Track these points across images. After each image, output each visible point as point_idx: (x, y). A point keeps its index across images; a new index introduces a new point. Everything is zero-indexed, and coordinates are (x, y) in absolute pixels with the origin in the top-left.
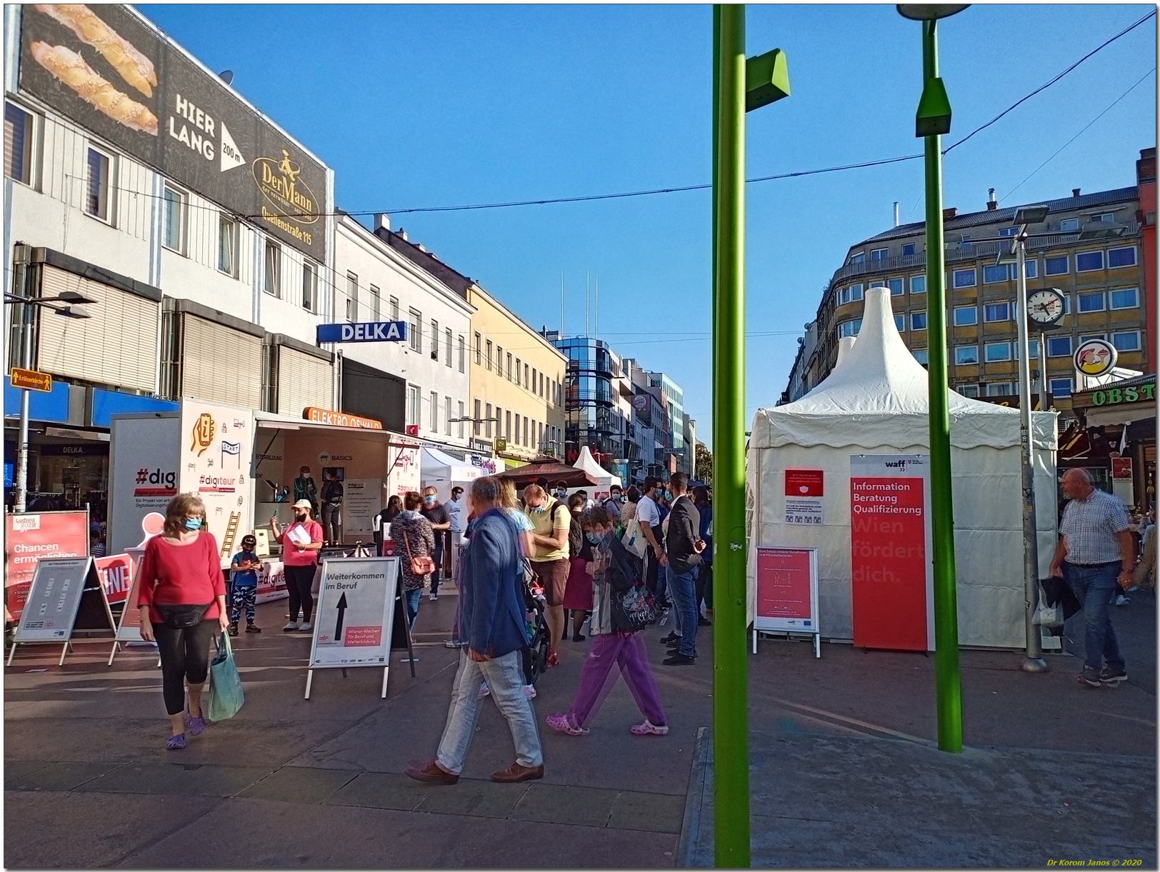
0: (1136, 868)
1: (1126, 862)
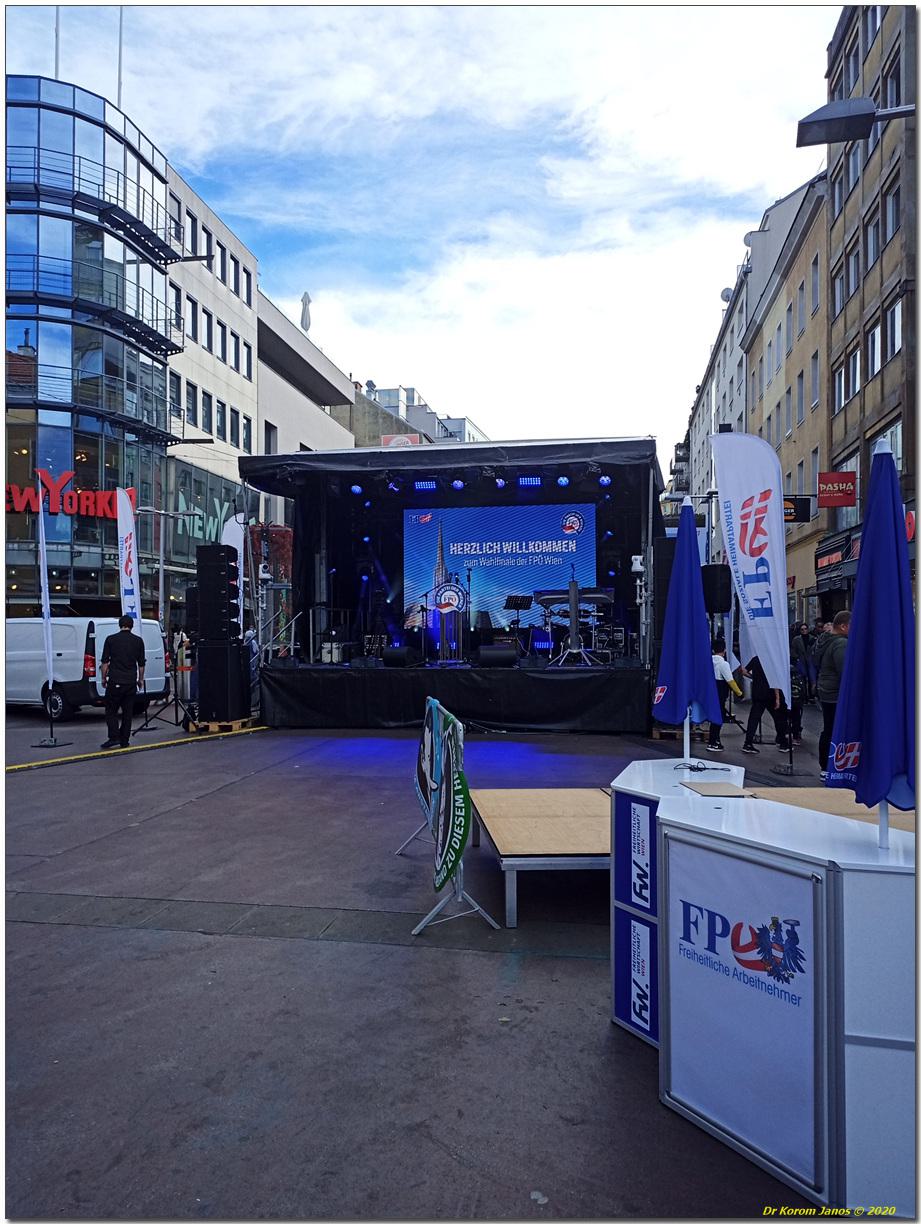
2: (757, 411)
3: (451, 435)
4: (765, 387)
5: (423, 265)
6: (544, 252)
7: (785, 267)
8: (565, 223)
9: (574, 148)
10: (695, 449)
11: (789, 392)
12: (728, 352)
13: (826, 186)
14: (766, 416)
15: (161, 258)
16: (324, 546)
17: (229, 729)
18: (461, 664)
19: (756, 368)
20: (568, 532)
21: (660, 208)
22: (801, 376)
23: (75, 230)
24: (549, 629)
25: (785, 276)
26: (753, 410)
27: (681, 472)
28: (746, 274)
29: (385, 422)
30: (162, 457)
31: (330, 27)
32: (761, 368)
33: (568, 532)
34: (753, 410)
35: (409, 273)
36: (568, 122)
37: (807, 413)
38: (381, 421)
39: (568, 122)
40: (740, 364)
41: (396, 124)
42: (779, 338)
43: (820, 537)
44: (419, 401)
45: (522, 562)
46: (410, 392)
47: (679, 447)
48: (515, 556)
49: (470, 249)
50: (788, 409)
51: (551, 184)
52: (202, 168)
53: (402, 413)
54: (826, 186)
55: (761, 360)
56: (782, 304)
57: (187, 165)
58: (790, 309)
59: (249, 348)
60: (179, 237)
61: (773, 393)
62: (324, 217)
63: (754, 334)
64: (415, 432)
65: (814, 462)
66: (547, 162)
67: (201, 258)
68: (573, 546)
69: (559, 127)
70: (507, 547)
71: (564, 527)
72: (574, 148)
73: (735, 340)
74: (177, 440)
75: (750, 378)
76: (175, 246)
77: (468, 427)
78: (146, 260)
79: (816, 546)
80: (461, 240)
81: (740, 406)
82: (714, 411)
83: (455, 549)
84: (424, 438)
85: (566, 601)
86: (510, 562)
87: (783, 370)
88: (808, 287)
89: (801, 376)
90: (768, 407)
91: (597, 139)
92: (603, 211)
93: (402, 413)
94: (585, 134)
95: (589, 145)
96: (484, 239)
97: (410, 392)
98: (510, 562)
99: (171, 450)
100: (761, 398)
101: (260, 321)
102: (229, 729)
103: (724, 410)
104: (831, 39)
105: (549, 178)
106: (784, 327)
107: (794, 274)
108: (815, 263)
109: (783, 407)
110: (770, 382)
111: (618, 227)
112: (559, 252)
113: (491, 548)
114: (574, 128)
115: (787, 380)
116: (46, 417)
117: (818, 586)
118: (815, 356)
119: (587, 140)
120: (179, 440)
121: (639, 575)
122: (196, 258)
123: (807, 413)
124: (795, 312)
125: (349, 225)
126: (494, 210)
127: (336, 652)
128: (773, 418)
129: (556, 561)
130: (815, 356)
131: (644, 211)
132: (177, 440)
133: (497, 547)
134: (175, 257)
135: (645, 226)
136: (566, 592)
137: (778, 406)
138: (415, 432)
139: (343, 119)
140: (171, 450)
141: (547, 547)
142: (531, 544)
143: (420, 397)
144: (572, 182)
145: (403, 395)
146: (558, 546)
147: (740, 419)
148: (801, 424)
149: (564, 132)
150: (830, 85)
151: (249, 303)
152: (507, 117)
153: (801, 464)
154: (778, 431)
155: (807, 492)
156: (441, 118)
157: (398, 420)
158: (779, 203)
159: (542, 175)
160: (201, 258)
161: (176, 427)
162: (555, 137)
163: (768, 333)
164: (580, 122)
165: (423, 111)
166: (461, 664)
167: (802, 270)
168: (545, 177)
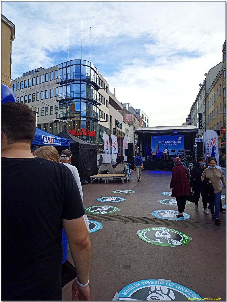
0: (219, 300)
1: (216, 299)
2: (208, 111)
3: (137, 113)
4: (210, 107)
5: (118, 71)
6: (146, 67)
7: (214, 84)
8: (151, 60)
9: (152, 42)
10: (192, 117)
11: (215, 109)
12: (201, 98)
13: (222, 72)
14: (210, 113)
15: (97, 88)
16: (141, 142)
17: (133, 170)
18: (167, 161)
19: (208, 102)
20: (179, 140)
21: (174, 55)
22: (218, 106)
23: (86, 86)
24: (178, 155)
25: (214, 86)
26: (207, 111)
27: (189, 121)
28: (205, 83)
29: (125, 112)
30: (97, 124)
31: (94, 17)
32: (209, 103)
33: (179, 140)
34: (207, 111)
35: (115, 73)
36: (151, 36)
37: (219, 114)
38: (124, 111)
39: (151, 36)
40: (204, 101)
41: (110, 38)
42: (213, 97)
43: (222, 138)
44: (130, 106)
45: (171, 144)
46: (129, 104)
47: (188, 116)
48: (170, 143)
49: (129, 66)
50: (215, 112)
51: (147, 50)
52: (66, 50)
53: (127, 109)
54: (222, 72)
55: (209, 101)
56: (213, 92)
57: (63, 50)
58: (215, 93)
59: (108, 102)
60: (101, 87)
61: (212, 109)
62: (94, 61)
63: (207, 97)
64: (132, 114)
65: (220, 124)
66: (146, 45)
67: (104, 88)
68: (180, 142)
69: (148, 37)
70: (169, 142)
71: (179, 139)
72: (152, 42)
73: (202, 99)
74: (100, 121)
75: (206, 104)
76: (100, 87)
77: (141, 111)
78: (95, 89)
79: (221, 140)
80: (126, 64)
81: (204, 109)
82: (197, 109)
83: (160, 142)
84: (134, 115)
85: (184, 151)
86: (169, 144)
87: (214, 104)
88: (219, 90)
89: (218, 106)
90: (211, 111)
91: (157, 40)
92: (160, 57)
93: (127, 109)
94: (155, 38)
95: (156, 41)
96: (132, 64)
97: (129, 104)
98: (169, 144)
99: (99, 123)
100: (209, 109)
101: (110, 97)
102: (133, 170)
103: (200, 109)
104: (223, 44)
105: (146, 49)
106: (214, 96)
107: (216, 86)
108: (220, 85)
109: (214, 112)
110: (211, 106)
111: (164, 60)
112: (150, 66)
113: (166, 142)
114: (152, 37)
115: (215, 107)
116: (82, 119)
117: (221, 148)
118: (220, 103)
119: (155, 40)
120: (100, 121)
121: (195, 148)
122: (103, 88)
123: (219, 114)
124: (216, 94)
125: (100, 62)
126: (134, 57)
127: (144, 159)
128: (212, 113)
129: (177, 144)
130: (220, 103)
131: (170, 56)
132: (100, 121)
133: (167, 142)
134: (100, 88)
135: (170, 60)
136: (184, 150)
137: (213, 111)
138: (132, 114)
139: (98, 38)
140: (99, 123)
141: (176, 142)
142: (173, 142)
143: (130, 105)
144: (152, 50)
145: (127, 105)
146: (178, 142)
147: (204, 112)
148: (217, 116)
149: (150, 38)
150: (223, 53)
151: (108, 93)
152: (136, 35)
153: (218, 124)
154: (213, 116)
155: (219, 130)
156: (120, 37)
157: (126, 110)
158: (212, 68)
159: (145, 49)
160: (104, 88)
161: (99, 119)
162: (148, 40)
163: (210, 96)
164: (153, 36)
165: (116, 35)
166: (167, 161)
167: (217, 86)
168: (146, 49)
